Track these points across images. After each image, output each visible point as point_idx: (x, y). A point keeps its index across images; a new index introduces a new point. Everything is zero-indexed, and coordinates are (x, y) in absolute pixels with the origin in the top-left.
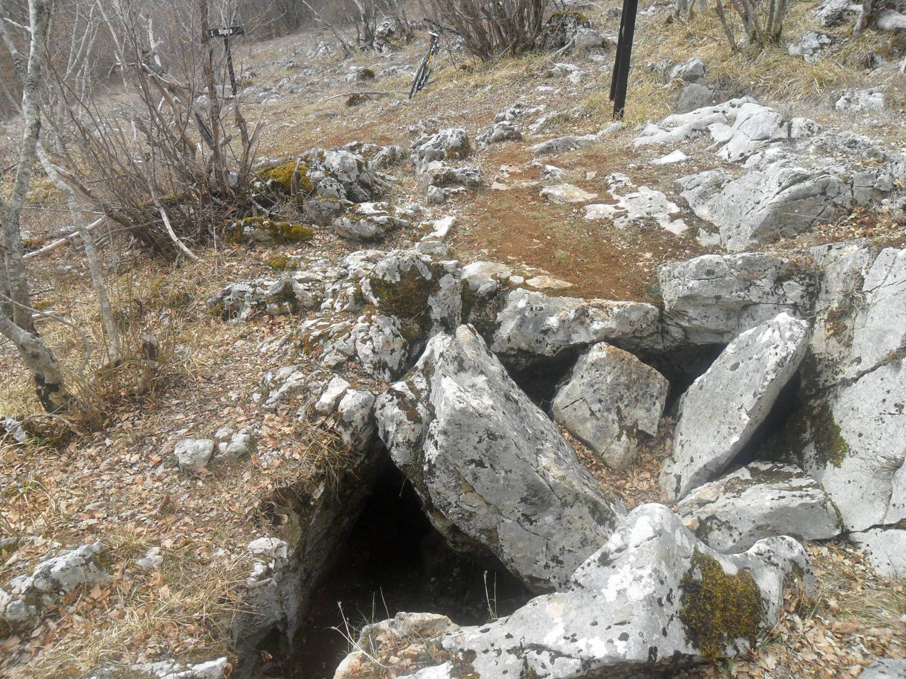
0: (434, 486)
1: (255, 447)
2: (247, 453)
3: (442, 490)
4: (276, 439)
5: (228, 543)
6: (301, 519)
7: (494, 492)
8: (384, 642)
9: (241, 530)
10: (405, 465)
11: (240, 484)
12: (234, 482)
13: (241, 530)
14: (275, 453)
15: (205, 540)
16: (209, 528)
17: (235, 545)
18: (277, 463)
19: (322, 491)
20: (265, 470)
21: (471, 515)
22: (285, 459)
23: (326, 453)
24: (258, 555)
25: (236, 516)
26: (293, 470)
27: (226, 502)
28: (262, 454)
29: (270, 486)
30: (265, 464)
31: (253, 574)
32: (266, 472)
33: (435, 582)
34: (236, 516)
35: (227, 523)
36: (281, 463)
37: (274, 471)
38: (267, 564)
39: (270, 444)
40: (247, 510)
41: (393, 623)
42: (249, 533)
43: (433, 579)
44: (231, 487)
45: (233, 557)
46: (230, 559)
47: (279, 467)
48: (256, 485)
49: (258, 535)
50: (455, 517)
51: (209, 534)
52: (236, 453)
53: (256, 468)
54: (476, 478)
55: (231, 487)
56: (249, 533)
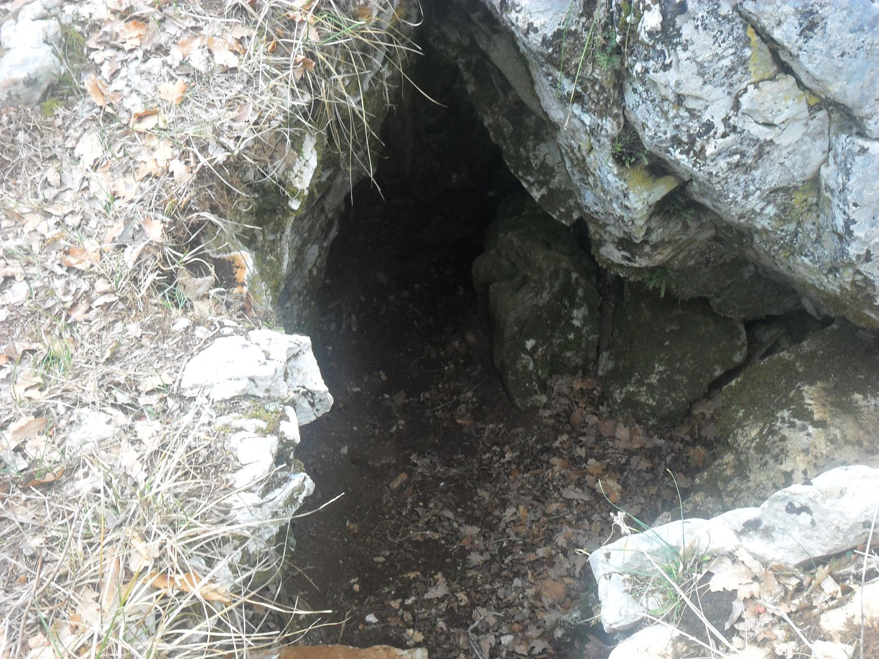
0: (671, 76)
1: (82, 59)
2: (64, 80)
3: (692, 85)
4: (143, 20)
5: (109, 386)
6: (260, 261)
7: (860, 61)
8: (743, 593)
9: (134, 329)
10: (558, 34)
11: (73, 180)
12: (52, 175)
13: (134, 329)
14: (155, 63)
15: (19, 390)
16: (20, 346)
17: (132, 385)
18: (173, 91)
19: (314, 162)
20: (140, 118)
21: (763, 149)
22: (195, 76)
23: (314, 37)
24: (232, 404)
25: (101, 285)
26: (231, 104)
27: (48, 244)
28: (115, 74)
29: (178, 167)
30: (135, 105)
31: (241, 479)
32: (149, 123)
33: (535, 349)
34: (101, 285)
35: (78, 314)
36: (188, 88)
37: (171, 116)
38: (274, 430)
39: (130, 35)
40: (130, 256)
41: (752, 526)
42: (166, 335)
43: (530, 344)
44: (50, 193)
45: (147, 429)
46: (136, 442)
47: (184, 101)
48: (127, 171)
49: (201, 332)
50: (722, 163)
51: (26, 367)
52: (31, 82)
53: (109, 118)
54: (812, 26)
55: (50, 193)
56: (166, 335)
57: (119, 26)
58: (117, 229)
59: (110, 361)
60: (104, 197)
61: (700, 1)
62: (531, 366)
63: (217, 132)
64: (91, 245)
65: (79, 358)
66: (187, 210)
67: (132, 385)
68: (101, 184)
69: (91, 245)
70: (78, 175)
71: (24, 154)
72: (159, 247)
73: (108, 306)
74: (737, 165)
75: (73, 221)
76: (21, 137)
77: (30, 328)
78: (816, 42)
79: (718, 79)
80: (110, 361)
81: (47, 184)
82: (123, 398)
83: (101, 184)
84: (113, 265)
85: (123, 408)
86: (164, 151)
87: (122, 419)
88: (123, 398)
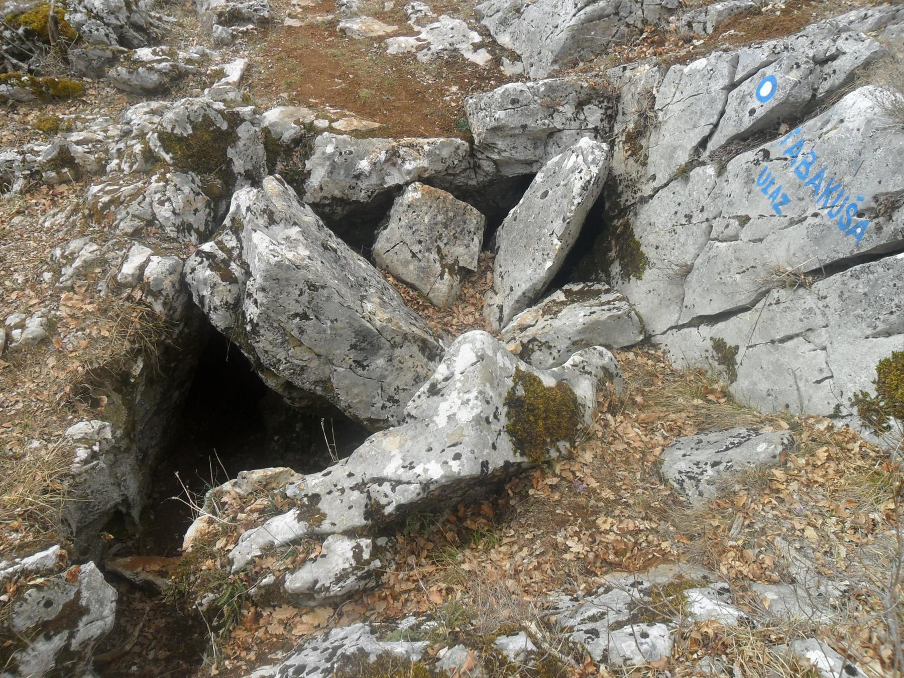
0: (261, 345)
3: (269, 348)
4: (78, 318)
5: (42, 434)
10: (226, 328)
13: (54, 418)
14: (79, 333)
16: (17, 422)
17: (50, 434)
18: (84, 343)
20: (71, 352)
21: (303, 369)
24: (79, 440)
25: (46, 405)
26: (104, 349)
27: (32, 391)
28: (65, 337)
29: (80, 369)
30: (70, 347)
31: (77, 460)
32: (74, 354)
33: (278, 440)
34: (46, 405)
38: (90, 448)
39: (73, 324)
40: (58, 397)
42: (64, 420)
43: (276, 438)
47: (87, 347)
52: (34, 339)
53: (60, 352)
54: (302, 332)
56: (64, 420)
57: (70, 320)
58: (55, 388)
59: (44, 427)
60: (53, 378)
61: (900, 152)
62: (276, 448)
63: (97, 358)
64: (46, 393)
65: (35, 425)
66: (81, 383)
67: (50, 434)
68: (53, 373)
69: (46, 393)
70: (46, 370)
71: (29, 362)
72: (68, 394)
73: (47, 411)
74: (294, 373)
75: (41, 385)
76: (29, 356)
77: (21, 416)
78: (305, 337)
79: (279, 345)
80: (44, 427)
81: (35, 372)
82: (46, 437)
83: (53, 373)
84: (51, 399)
85: (46, 440)
86: (77, 363)
87: (44, 443)
88: (46, 437)
